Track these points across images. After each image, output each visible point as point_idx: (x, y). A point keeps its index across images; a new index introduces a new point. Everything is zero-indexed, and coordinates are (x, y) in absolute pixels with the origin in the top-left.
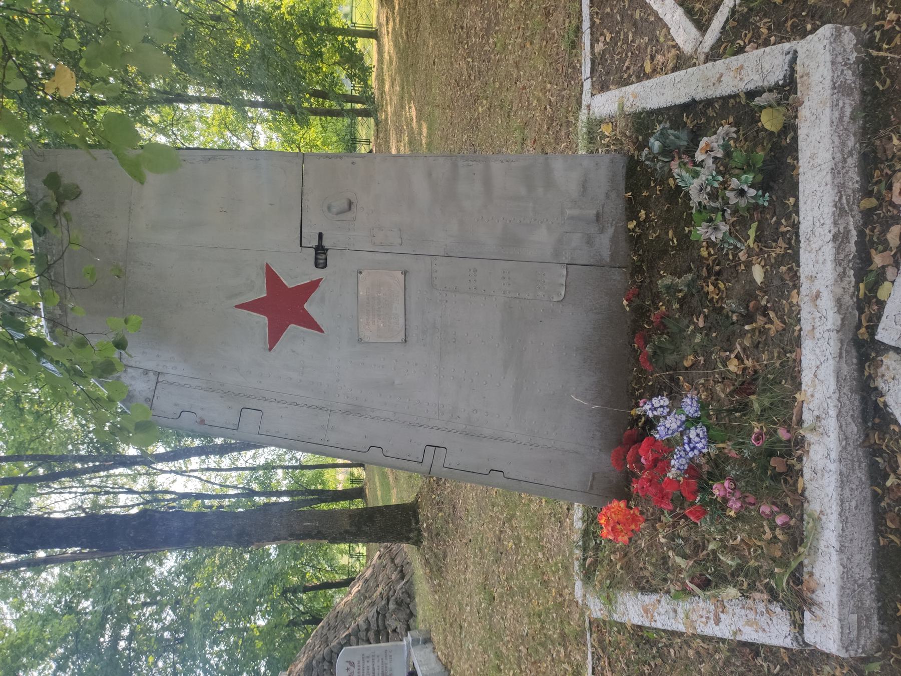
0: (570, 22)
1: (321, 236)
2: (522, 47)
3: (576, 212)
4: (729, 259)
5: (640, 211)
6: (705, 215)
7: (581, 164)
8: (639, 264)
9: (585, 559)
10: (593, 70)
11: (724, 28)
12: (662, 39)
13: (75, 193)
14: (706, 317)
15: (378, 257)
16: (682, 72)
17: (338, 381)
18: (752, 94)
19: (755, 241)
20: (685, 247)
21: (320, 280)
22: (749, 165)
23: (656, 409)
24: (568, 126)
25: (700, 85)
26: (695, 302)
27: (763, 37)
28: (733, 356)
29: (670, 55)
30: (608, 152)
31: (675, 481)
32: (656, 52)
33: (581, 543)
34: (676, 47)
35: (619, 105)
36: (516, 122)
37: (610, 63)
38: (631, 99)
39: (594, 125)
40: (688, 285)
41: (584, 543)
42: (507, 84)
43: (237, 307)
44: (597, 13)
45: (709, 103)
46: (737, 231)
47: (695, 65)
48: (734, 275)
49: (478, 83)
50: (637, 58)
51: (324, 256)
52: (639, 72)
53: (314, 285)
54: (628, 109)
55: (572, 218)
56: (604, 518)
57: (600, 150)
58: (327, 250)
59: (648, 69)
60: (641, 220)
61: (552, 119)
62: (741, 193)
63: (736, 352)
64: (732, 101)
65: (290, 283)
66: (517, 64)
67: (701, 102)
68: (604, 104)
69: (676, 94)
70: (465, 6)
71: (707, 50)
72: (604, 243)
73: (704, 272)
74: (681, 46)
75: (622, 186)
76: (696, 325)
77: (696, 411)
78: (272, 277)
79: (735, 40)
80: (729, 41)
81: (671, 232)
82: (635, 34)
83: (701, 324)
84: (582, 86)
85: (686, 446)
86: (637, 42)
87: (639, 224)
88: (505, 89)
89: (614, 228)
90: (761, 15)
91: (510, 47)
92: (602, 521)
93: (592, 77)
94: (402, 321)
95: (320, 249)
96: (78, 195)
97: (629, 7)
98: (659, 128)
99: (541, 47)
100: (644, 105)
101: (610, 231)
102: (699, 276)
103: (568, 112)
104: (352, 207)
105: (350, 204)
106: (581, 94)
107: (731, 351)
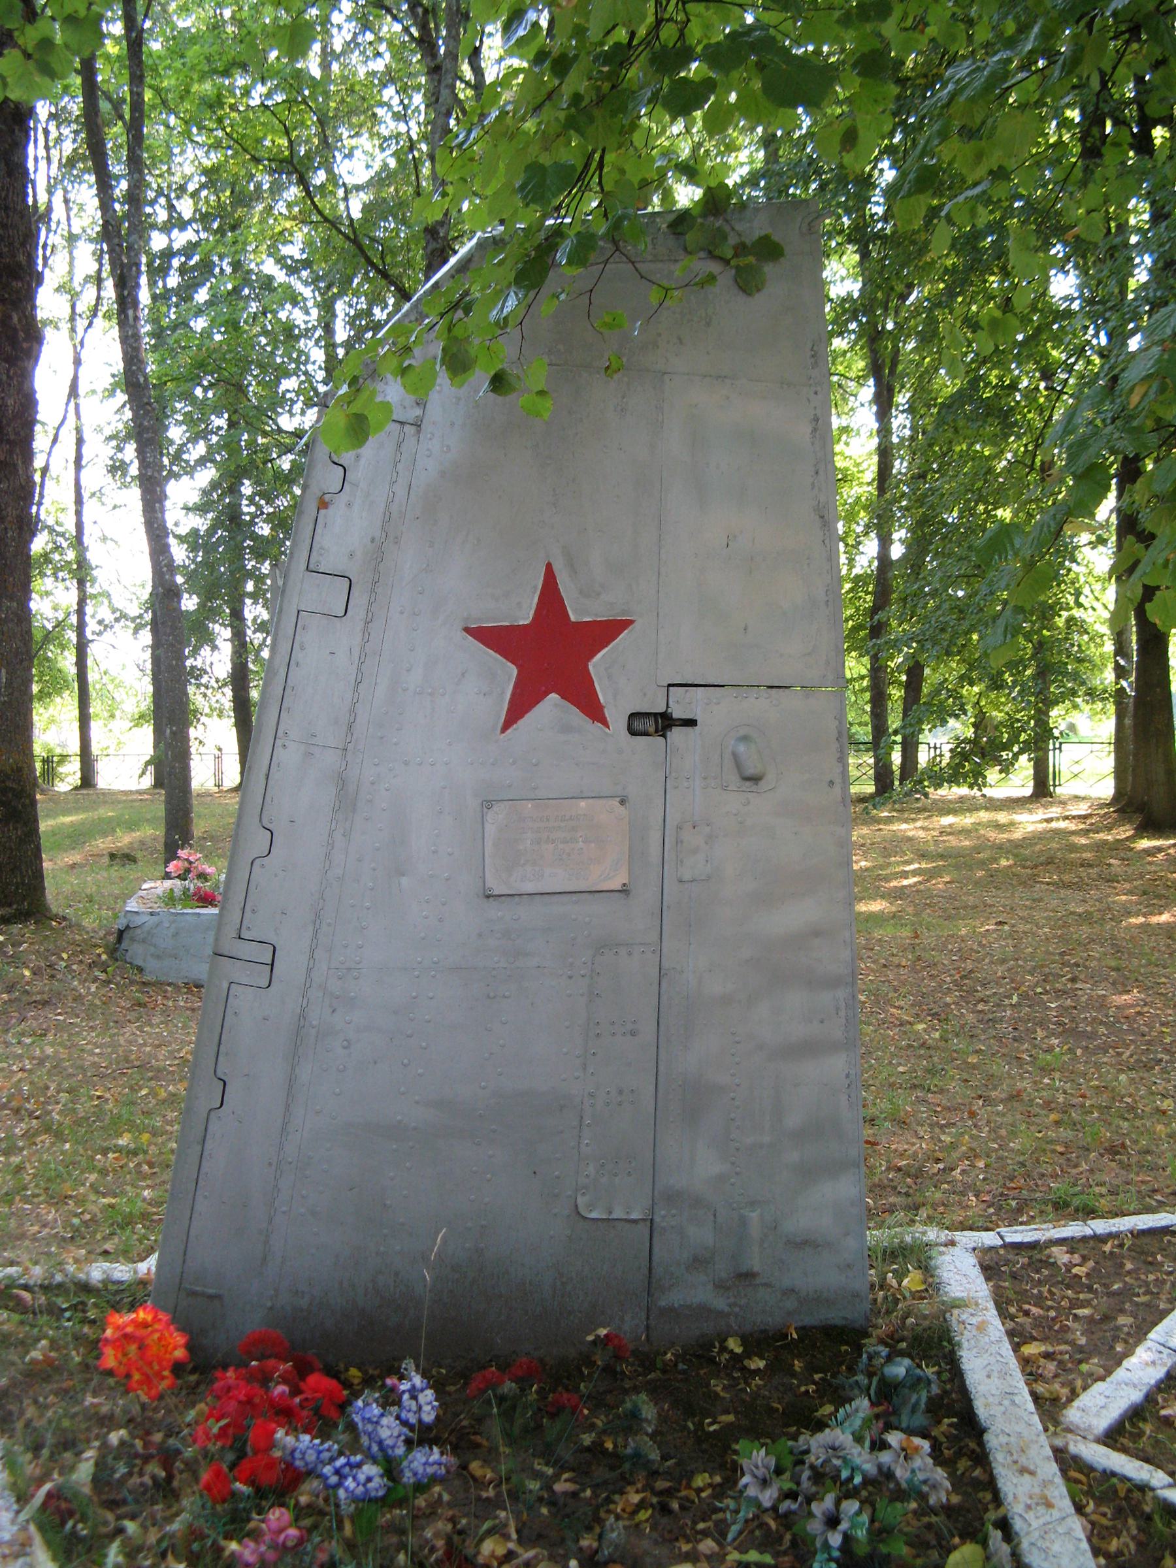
0: (1102, 1196)
1: (691, 723)
2: (1048, 1105)
3: (755, 1230)
4: (695, 1523)
5: (762, 1358)
6: (788, 1461)
7: (847, 1234)
8: (659, 1365)
9: (26, 1287)
10: (1018, 1247)
11: (1113, 1474)
12: (1084, 1367)
13: (747, 283)
14: (575, 1495)
15: (655, 836)
16: (1031, 1406)
17: (406, 763)
18: (1004, 1525)
19: (740, 1563)
20: (704, 1446)
21: (605, 723)
22: (880, 1532)
23: (414, 1398)
24: (908, 1208)
25: (1012, 1439)
26: (601, 1473)
27: (1103, 1545)
28: (511, 1545)
29: (1057, 1386)
30: (872, 1286)
31: (272, 1444)
32: (1060, 1362)
33: (59, 1278)
34: (1074, 1395)
35: (962, 1299)
36: (906, 1103)
37: (1033, 1279)
38: (974, 1321)
39: (919, 1257)
40: (637, 1455)
41: (60, 1286)
42: (977, 1079)
43: (549, 567)
44: (1121, 1246)
45: (982, 1458)
46: (752, 1532)
47: (1046, 1430)
48: (667, 1536)
49: (971, 1018)
50: (1049, 1330)
51: (652, 729)
52: (1020, 1335)
53: (594, 711)
54: (955, 1316)
55: (743, 1222)
56: (149, 1318)
57: (872, 1272)
58: (664, 736)
59: (1030, 1349)
60: (746, 1362)
61: (918, 1174)
62: (833, 1521)
63: (520, 1550)
64: (989, 1496)
65: (597, 665)
66: (1015, 1096)
67: (981, 1444)
68: (960, 1272)
69: (991, 1399)
70: (1114, 984)
71: (1072, 1449)
72: (698, 1292)
73: (661, 1485)
74: (1075, 1404)
75: (808, 1321)
76: (556, 1477)
77: (415, 1474)
78: (607, 631)
79: (1093, 1497)
80: (1090, 1486)
81: (730, 1418)
82: (1090, 1320)
83: (559, 1487)
84: (987, 1229)
85: (342, 1460)
86: (1076, 1325)
87: (735, 1357)
88: (965, 1076)
89: (727, 1309)
90: (1142, 1537)
91: (1046, 1081)
92: (142, 1315)
93: (1006, 1246)
94: (529, 887)
95: (664, 723)
96: (744, 291)
97: (1137, 1304)
98: (930, 1372)
99: (1052, 1142)
100: (965, 1345)
101: (720, 1303)
102: (654, 1474)
103: (934, 1206)
104: (748, 783)
105: (755, 779)
106: (971, 1229)
107: (520, 1541)
